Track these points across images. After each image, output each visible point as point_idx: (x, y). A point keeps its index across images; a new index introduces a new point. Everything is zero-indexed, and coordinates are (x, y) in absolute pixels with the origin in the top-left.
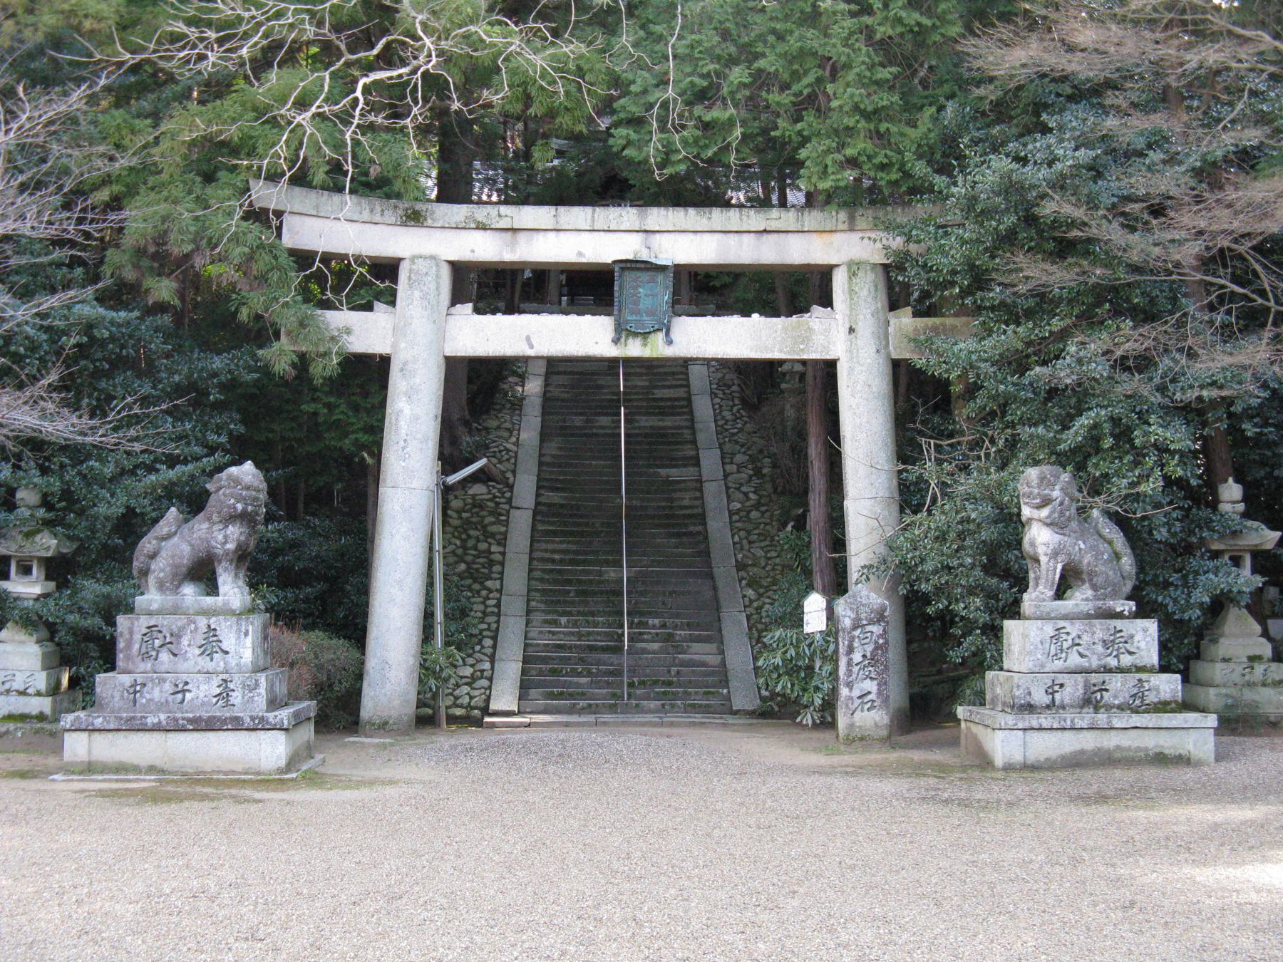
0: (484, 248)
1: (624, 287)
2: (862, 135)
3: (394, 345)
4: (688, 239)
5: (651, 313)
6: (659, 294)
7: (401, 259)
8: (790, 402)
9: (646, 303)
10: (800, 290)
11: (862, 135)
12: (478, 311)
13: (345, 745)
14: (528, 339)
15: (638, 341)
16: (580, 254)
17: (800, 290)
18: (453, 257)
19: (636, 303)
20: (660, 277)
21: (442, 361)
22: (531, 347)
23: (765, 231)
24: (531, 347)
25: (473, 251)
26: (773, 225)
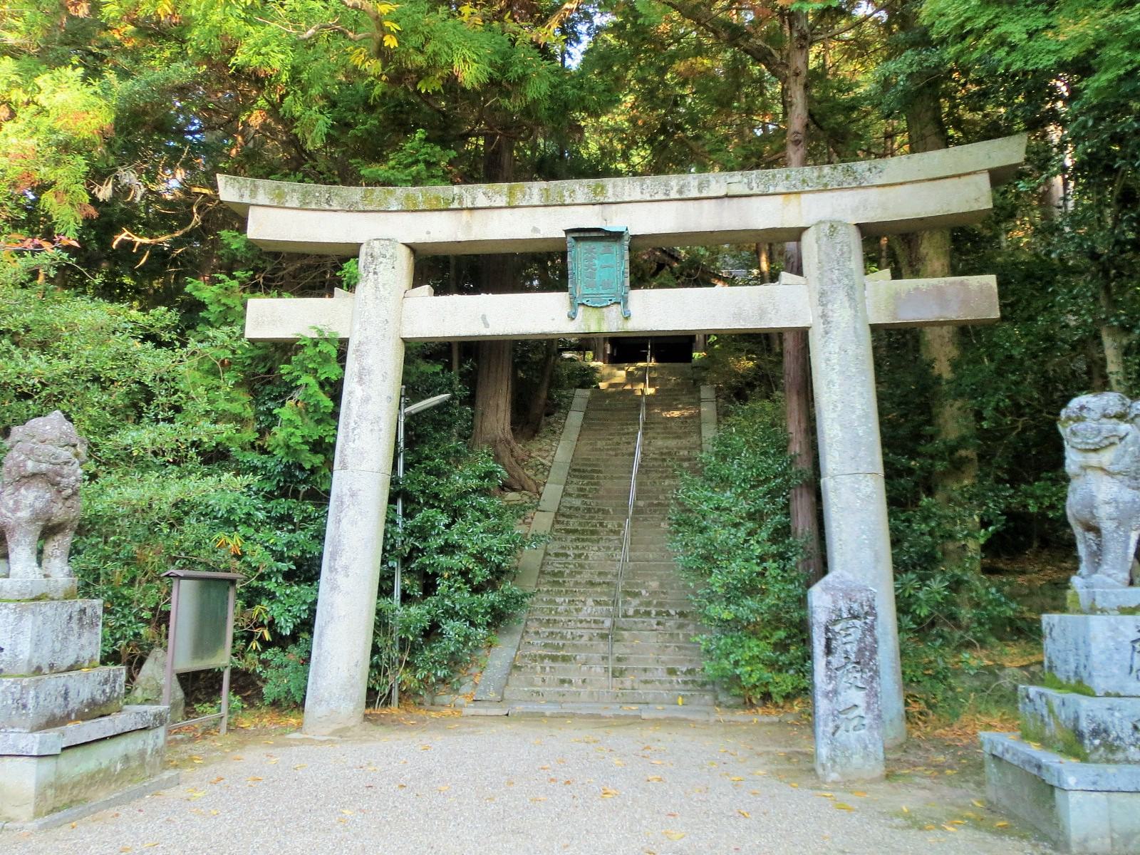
0: (442, 229)
1: (580, 259)
2: (803, 613)
3: (351, 331)
4: (652, 207)
5: (607, 285)
6: (615, 263)
7: (360, 245)
8: (766, 368)
9: (602, 275)
10: (773, 254)
11: (803, 613)
12: (438, 291)
13: (288, 745)
14: (484, 317)
15: (594, 314)
16: (535, 230)
17: (773, 254)
18: (410, 240)
19: (591, 276)
20: (615, 247)
21: (868, 327)
22: (487, 325)
23: (727, 196)
24: (487, 325)
25: (428, 233)
26: (735, 189)
